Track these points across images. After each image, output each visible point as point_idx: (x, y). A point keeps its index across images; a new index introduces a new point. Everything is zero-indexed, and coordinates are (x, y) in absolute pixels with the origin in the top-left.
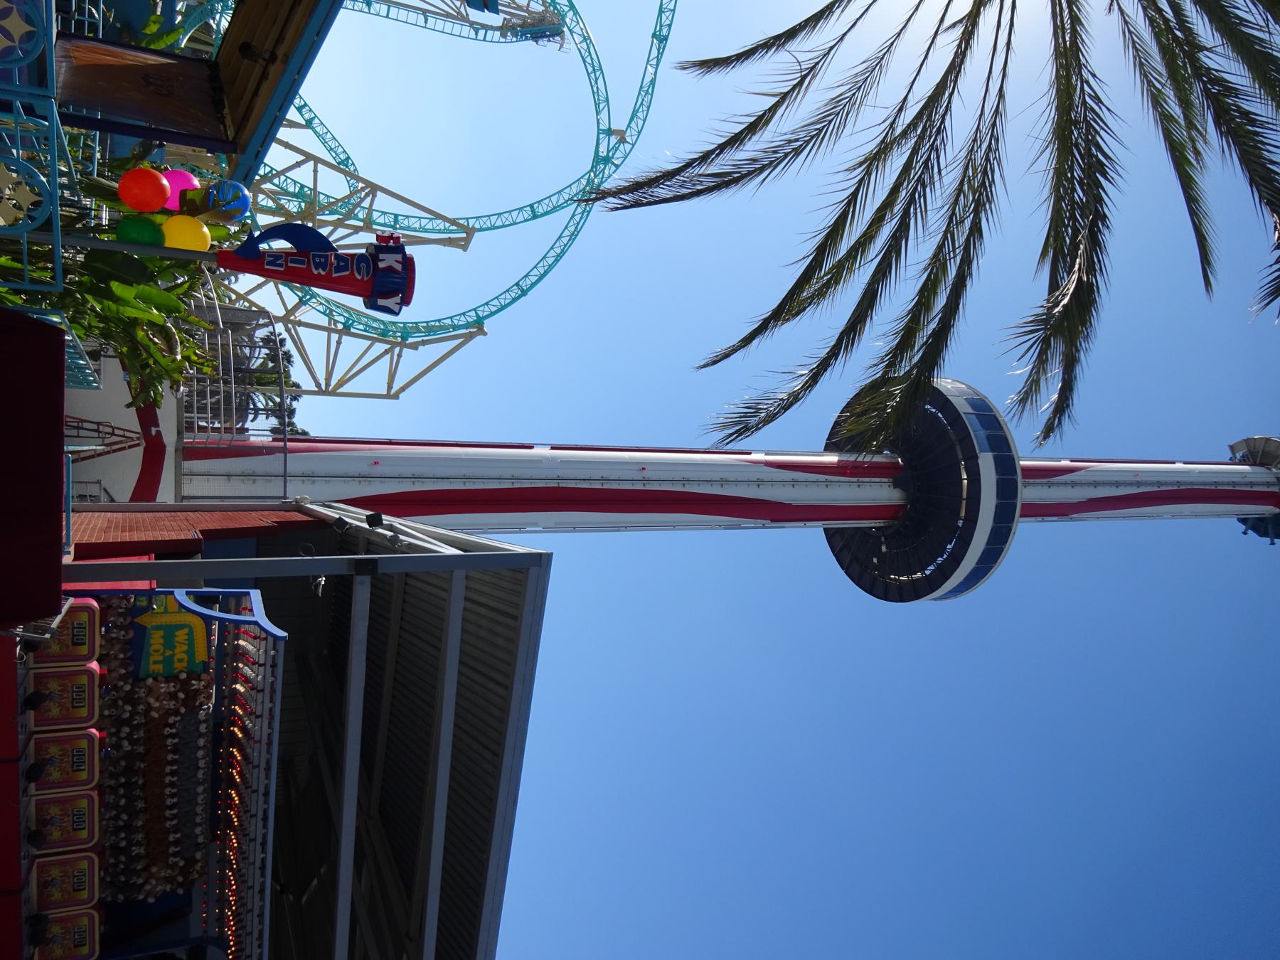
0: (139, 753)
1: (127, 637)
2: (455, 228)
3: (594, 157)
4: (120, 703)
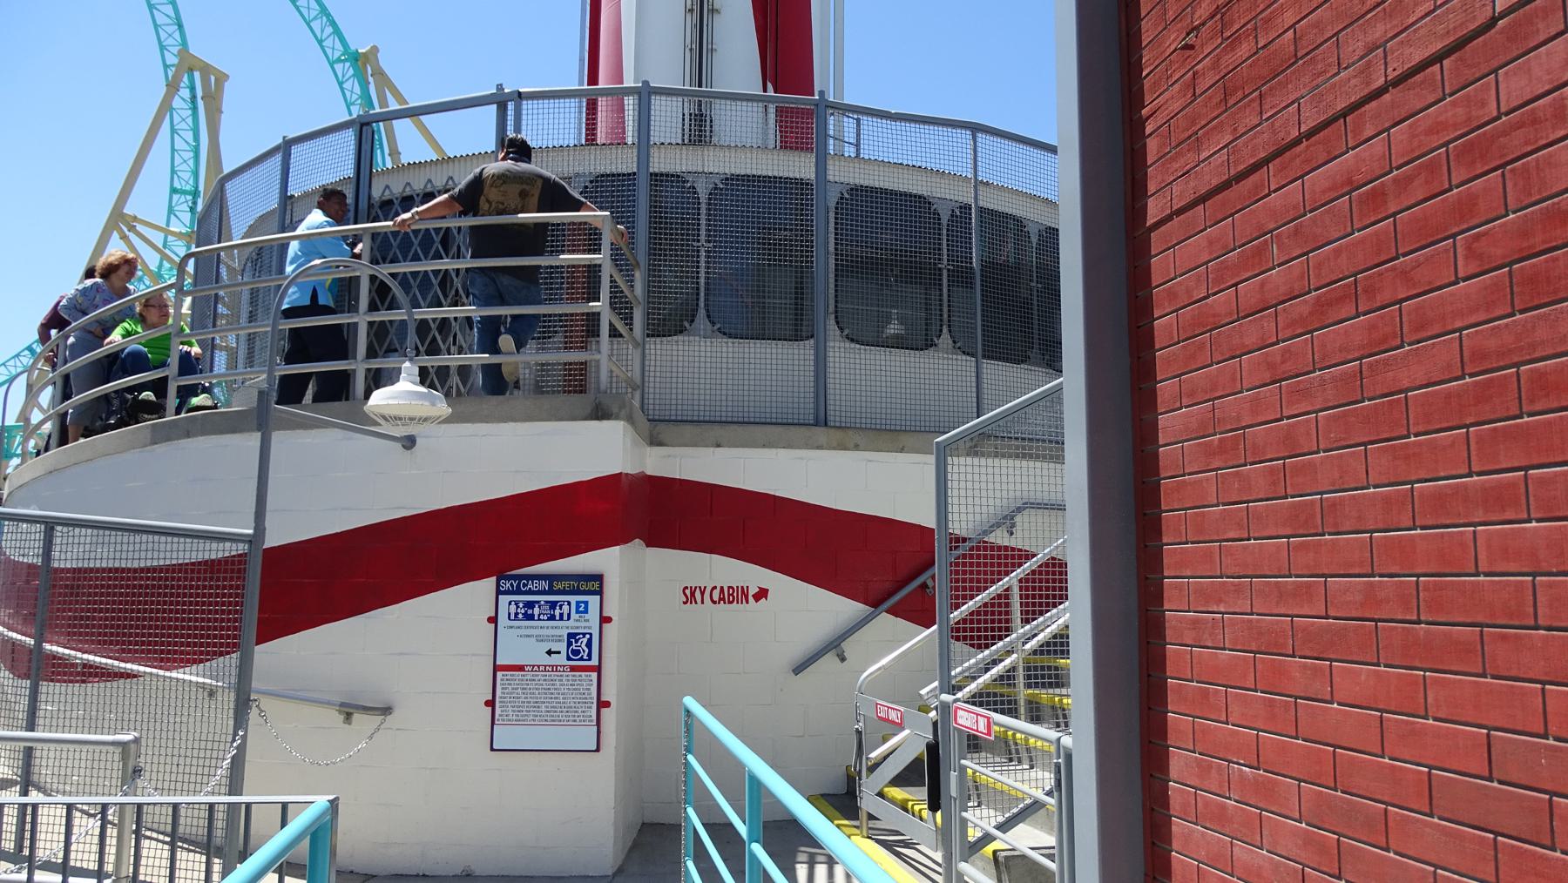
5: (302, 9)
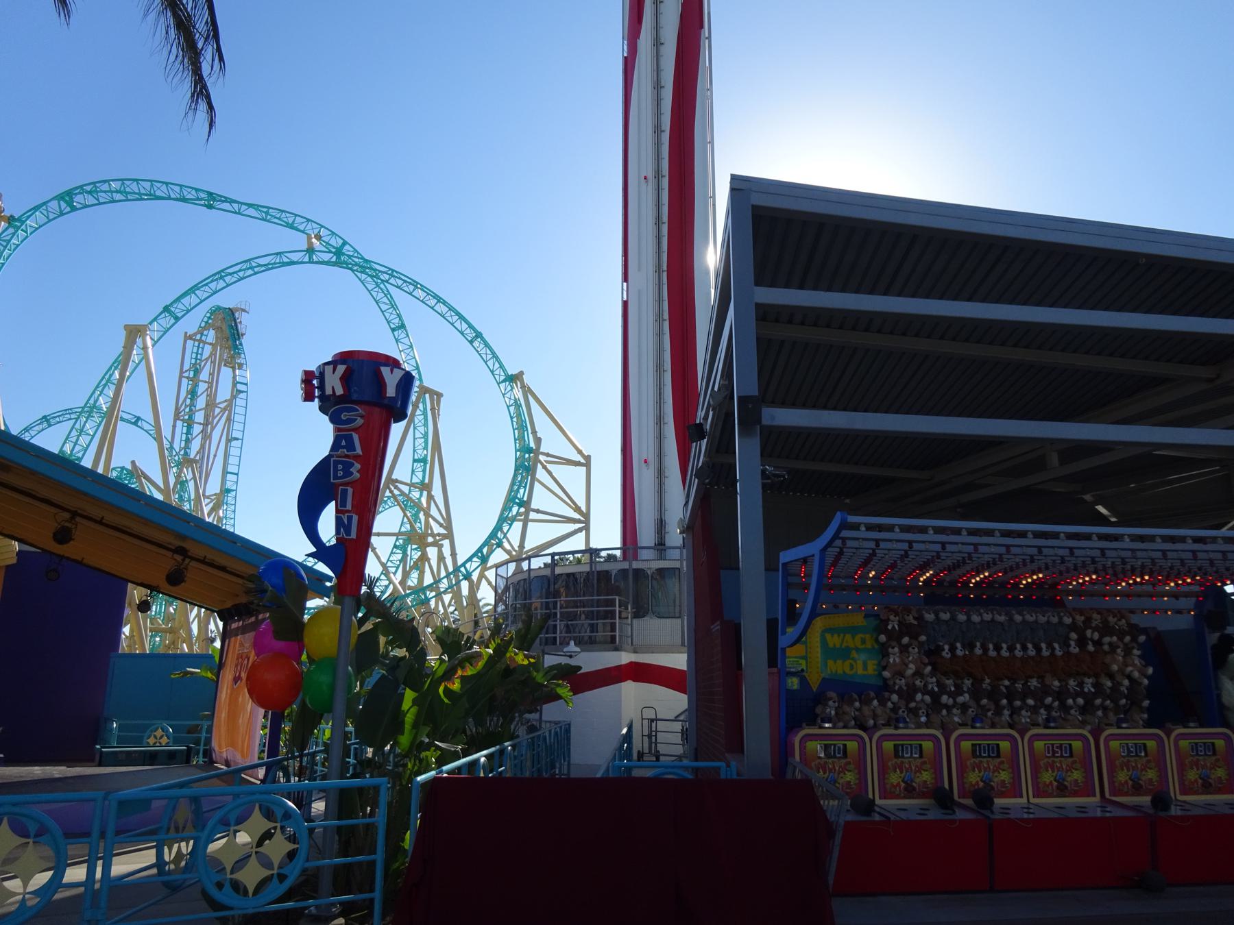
0: (972, 684)
1: (836, 699)
2: (421, 406)
3: (338, 266)
4: (913, 705)
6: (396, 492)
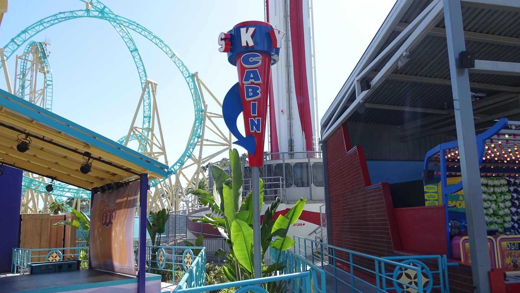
5: (184, 74)
6: (137, 133)
